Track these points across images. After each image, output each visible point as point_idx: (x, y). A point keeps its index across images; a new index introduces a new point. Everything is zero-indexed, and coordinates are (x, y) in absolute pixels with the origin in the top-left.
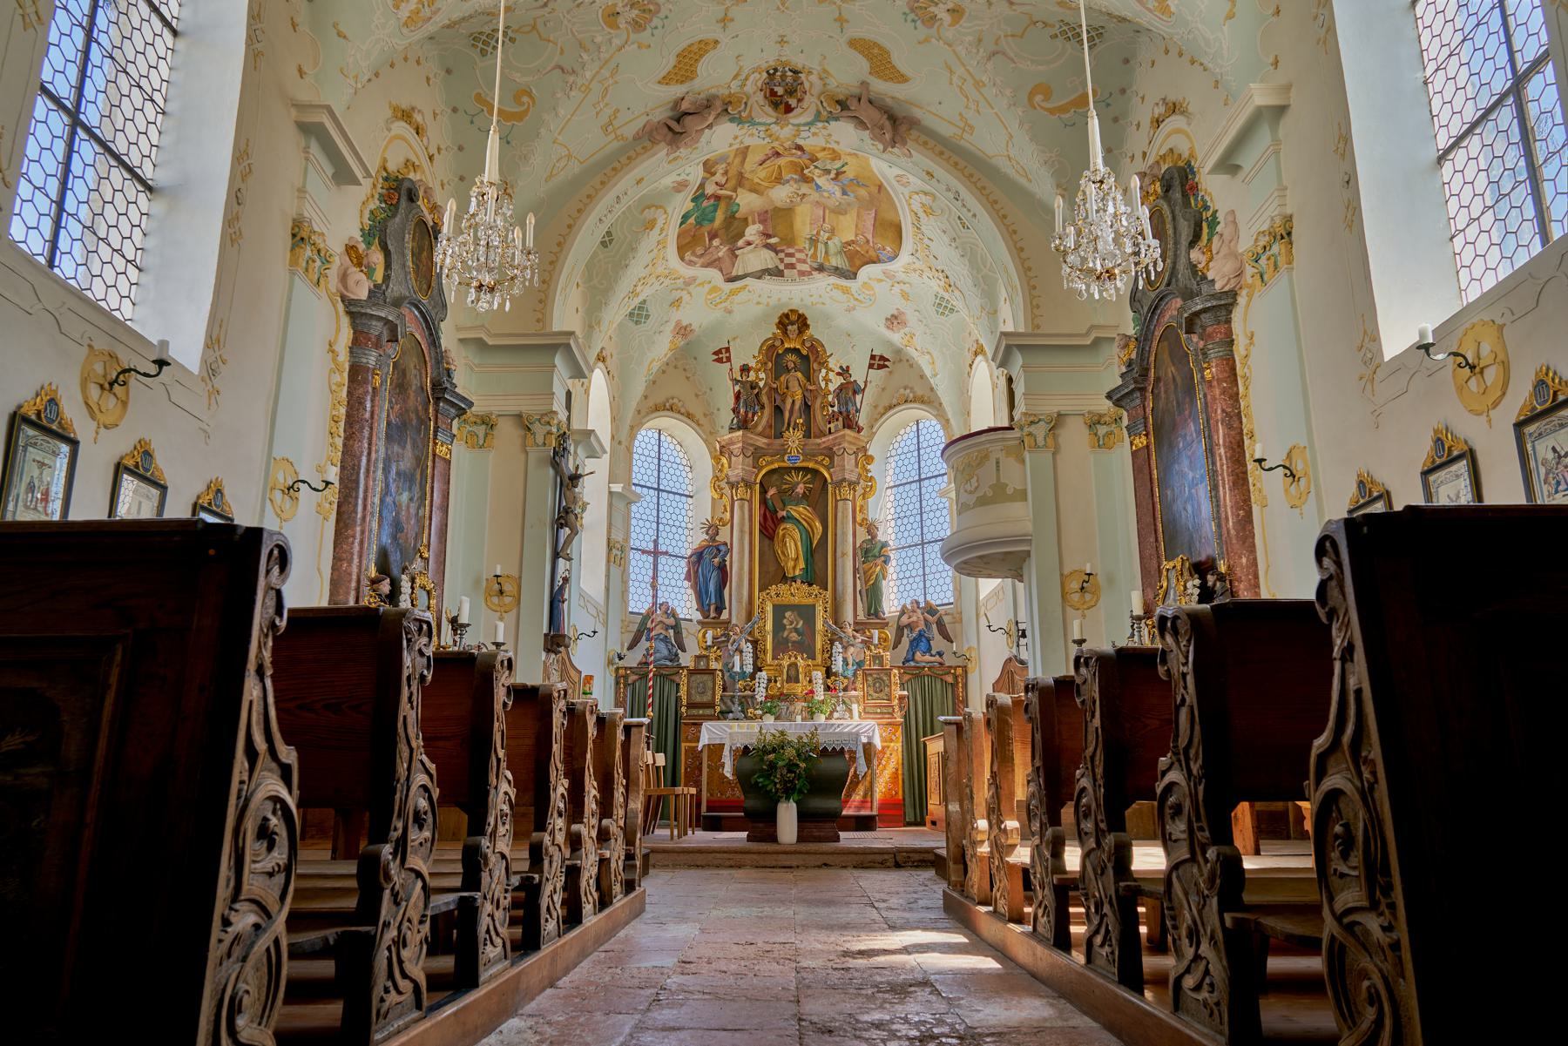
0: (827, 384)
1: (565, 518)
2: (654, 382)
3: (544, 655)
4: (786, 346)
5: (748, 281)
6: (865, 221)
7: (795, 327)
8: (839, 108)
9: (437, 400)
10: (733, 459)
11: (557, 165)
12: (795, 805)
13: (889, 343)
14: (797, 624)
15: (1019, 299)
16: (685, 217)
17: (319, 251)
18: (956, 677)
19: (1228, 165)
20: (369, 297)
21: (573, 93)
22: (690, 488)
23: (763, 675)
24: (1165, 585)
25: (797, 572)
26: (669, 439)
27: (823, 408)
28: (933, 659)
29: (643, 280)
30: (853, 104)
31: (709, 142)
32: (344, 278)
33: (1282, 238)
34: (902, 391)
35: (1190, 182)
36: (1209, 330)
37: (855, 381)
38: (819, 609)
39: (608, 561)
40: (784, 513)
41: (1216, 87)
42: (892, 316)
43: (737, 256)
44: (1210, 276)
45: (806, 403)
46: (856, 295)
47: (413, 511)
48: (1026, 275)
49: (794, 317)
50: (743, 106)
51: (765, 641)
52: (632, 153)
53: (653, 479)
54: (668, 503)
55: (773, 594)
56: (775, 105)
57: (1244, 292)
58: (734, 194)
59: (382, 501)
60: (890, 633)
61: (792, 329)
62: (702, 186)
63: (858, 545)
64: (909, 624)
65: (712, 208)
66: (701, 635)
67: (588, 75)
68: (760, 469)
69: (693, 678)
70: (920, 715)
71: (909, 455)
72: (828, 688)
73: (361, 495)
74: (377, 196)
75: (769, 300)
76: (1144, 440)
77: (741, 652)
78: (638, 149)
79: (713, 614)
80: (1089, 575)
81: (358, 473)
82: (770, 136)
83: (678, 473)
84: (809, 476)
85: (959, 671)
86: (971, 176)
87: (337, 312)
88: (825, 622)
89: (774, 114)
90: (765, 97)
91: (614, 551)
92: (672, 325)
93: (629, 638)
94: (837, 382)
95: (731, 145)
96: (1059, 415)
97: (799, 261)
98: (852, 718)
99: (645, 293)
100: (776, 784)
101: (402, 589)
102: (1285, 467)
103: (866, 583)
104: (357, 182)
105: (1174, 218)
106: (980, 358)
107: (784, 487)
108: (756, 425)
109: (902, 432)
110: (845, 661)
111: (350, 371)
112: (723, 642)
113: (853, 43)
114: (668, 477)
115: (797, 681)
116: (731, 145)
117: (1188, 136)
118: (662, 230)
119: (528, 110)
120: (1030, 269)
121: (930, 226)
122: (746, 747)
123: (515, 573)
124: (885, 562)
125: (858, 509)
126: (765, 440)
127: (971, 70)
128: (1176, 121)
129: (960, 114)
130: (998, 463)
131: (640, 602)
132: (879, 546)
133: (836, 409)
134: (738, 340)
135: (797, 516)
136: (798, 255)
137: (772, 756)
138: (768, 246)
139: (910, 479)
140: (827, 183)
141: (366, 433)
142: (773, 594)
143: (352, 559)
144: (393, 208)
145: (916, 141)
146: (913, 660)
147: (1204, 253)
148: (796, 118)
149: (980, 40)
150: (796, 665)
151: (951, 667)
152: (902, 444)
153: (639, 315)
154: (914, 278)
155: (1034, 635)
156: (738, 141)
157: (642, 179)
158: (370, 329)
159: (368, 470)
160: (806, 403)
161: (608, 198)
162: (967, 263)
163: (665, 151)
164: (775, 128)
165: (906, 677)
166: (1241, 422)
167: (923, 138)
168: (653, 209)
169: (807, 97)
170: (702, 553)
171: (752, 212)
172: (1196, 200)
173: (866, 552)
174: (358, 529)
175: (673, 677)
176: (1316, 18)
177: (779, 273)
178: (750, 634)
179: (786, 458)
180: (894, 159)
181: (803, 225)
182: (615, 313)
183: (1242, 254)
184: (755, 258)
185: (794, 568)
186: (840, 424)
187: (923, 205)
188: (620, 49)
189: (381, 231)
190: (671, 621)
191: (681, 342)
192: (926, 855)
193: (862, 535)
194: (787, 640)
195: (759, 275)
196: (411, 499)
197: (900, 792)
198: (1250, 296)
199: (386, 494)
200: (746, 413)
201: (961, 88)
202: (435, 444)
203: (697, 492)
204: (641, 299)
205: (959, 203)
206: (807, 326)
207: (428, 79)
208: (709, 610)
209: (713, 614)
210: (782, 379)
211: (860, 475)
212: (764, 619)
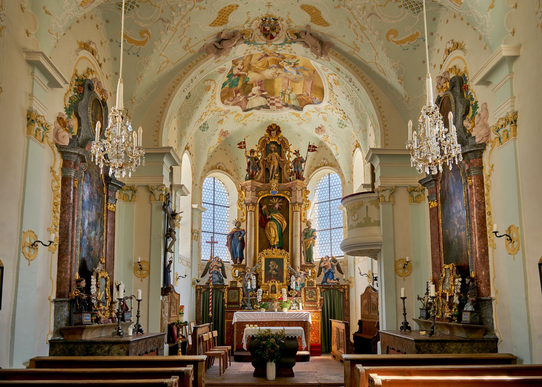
0: (289, 158)
1: (170, 234)
2: (211, 156)
3: (161, 297)
4: (271, 140)
5: (254, 111)
6: (307, 86)
7: (275, 132)
8: (296, 37)
9: (107, 184)
10: (247, 192)
11: (162, 66)
12: (274, 364)
13: (317, 139)
14: (275, 267)
15: (379, 131)
16: (224, 85)
17: (42, 125)
18: (344, 290)
19: (485, 81)
20: (70, 143)
21: (168, 32)
24: (444, 275)
25: (275, 243)
28: (334, 282)
29: (205, 114)
30: (303, 36)
31: (234, 53)
32: (56, 135)
33: (512, 123)
34: (322, 160)
35: (464, 85)
36: (471, 161)
37: (302, 157)
38: (285, 260)
39: (192, 239)
40: (270, 217)
41: (480, 39)
42: (319, 127)
43: (248, 100)
44: (473, 134)
46: (302, 118)
47: (97, 239)
48: (382, 120)
49: (274, 127)
50: (250, 36)
52: (198, 58)
53: (211, 200)
54: (218, 210)
55: (265, 253)
56: (266, 35)
57: (490, 144)
58: (247, 73)
59: (81, 239)
60: (316, 270)
61: (274, 133)
62: (232, 70)
63: (302, 231)
65: (236, 80)
66: (233, 271)
67: (176, 23)
68: (259, 197)
69: (230, 291)
70: (329, 306)
71: (325, 189)
72: (289, 296)
73: (70, 240)
74: (73, 90)
76: (435, 203)
77: (251, 279)
78: (201, 56)
79: (238, 262)
80: (408, 262)
81: (68, 230)
82: (263, 49)
83: (222, 196)
84: (281, 200)
85: (346, 287)
86: (358, 71)
87: (54, 152)
89: (265, 40)
90: (261, 31)
91: (194, 234)
92: (219, 131)
93: (201, 272)
95: (245, 54)
96: (396, 187)
97: (277, 102)
98: (299, 309)
99: (206, 118)
100: (266, 355)
101: (92, 283)
102: (507, 235)
104: (61, 87)
105: (455, 102)
106: (358, 149)
107: (270, 205)
108: (257, 177)
110: (296, 283)
111: (62, 180)
112: (243, 274)
113: (303, 7)
114: (218, 199)
116: (245, 54)
117: (464, 61)
118: (213, 91)
119: (147, 40)
120: (384, 117)
121: (337, 90)
122: (253, 336)
123: (147, 260)
124: (314, 239)
125: (302, 214)
126: (261, 184)
127: (360, 22)
128: (457, 53)
129: (354, 42)
130: (367, 208)
131: (206, 256)
133: (293, 170)
134: (249, 137)
135: (275, 218)
136: (276, 100)
137: (264, 342)
138: (262, 96)
139: (326, 200)
140: (290, 69)
141: (71, 210)
142: (265, 253)
143: (67, 271)
144: (81, 95)
145: (332, 53)
147: (470, 122)
148: (275, 42)
149: (364, 8)
150: (275, 285)
151: (342, 285)
152: (322, 184)
153: (204, 127)
154: (329, 112)
155: (381, 281)
156: (248, 52)
157: (203, 71)
158: (71, 159)
159: (73, 228)
161: (188, 80)
162: (354, 107)
163: (214, 58)
164: (265, 46)
165: (323, 290)
166: (485, 207)
167: (336, 52)
168: (209, 81)
169: (281, 32)
171: (255, 81)
172: (467, 94)
173: (306, 234)
174: (70, 257)
176: (537, 13)
177: (267, 107)
178: (255, 271)
179: (271, 192)
180: (322, 61)
181: (279, 86)
182: (192, 129)
183: (490, 127)
184: (257, 101)
185: (274, 241)
187: (334, 80)
188: (190, 10)
189: (75, 108)
190: (220, 265)
191: (223, 138)
193: (304, 226)
194: (271, 274)
195: (258, 108)
196: (96, 234)
197: (320, 341)
198: (493, 147)
199: (83, 235)
200: (253, 172)
201: (354, 30)
202: (107, 205)
204: (204, 122)
205: (352, 84)
206: (280, 132)
207: (97, 26)
208: (237, 260)
209: (238, 262)
210: (269, 156)
211: (303, 200)
212: (261, 265)
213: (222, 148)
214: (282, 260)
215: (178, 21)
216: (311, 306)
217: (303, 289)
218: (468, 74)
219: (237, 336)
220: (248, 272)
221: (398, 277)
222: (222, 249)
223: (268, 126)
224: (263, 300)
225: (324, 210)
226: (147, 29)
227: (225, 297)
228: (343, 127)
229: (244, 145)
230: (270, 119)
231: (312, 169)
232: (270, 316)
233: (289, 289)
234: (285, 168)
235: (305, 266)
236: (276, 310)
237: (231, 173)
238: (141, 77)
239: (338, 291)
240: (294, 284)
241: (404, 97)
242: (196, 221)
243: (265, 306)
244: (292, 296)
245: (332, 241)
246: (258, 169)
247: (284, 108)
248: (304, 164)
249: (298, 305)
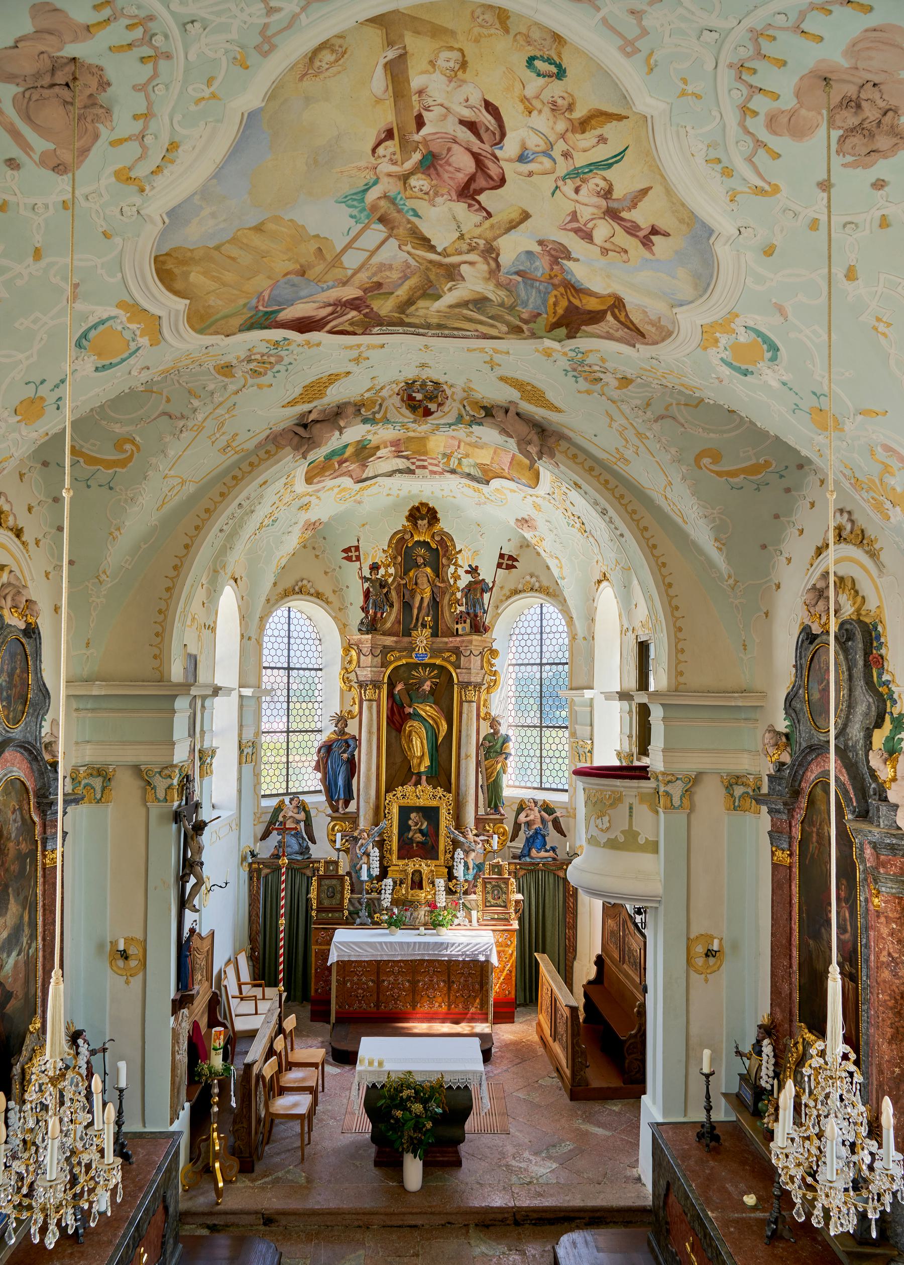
7: (425, 522)
14: (422, 825)
23: (389, 882)
26: (299, 615)
28: (547, 854)
34: (528, 578)
38: (443, 813)
39: (240, 763)
40: (411, 710)
42: (523, 519)
49: (424, 511)
50: (377, 408)
55: (399, 794)
70: (533, 907)
72: (450, 892)
77: (368, 855)
84: (436, 672)
86: (622, 496)
90: (403, 400)
93: (261, 829)
94: (465, 580)
97: (431, 464)
100: (402, 1144)
115: (421, 888)
123: (139, 936)
124: (506, 759)
125: (482, 703)
126: (394, 639)
130: (631, 808)
131: (272, 782)
132: (501, 741)
134: (367, 527)
135: (423, 714)
139: (532, 661)
142: (399, 794)
145: (566, 452)
146: (529, 855)
149: (648, 405)
167: (574, 450)
169: (448, 402)
170: (331, 745)
175: (304, 871)
186: (467, 626)
192: (544, 1214)
195: (391, 474)
197: (513, 992)
200: (375, 613)
202: (44, 856)
203: (325, 667)
206: (438, 520)
210: (411, 574)
213: (308, 545)
214: (436, 810)
215: (206, 414)
218: (884, 628)
219: (337, 991)
221: (694, 976)
223: (410, 508)
226: (131, 435)
227: (313, 895)
229: (357, 553)
230: (415, 491)
231: (504, 592)
232: (408, 948)
233: (451, 877)
234: (446, 601)
237: (327, 599)
238: (119, 529)
239: (555, 874)
240: (461, 868)
241: (726, 577)
242: (249, 719)
244: (456, 892)
247: (448, 475)
248: (488, 594)
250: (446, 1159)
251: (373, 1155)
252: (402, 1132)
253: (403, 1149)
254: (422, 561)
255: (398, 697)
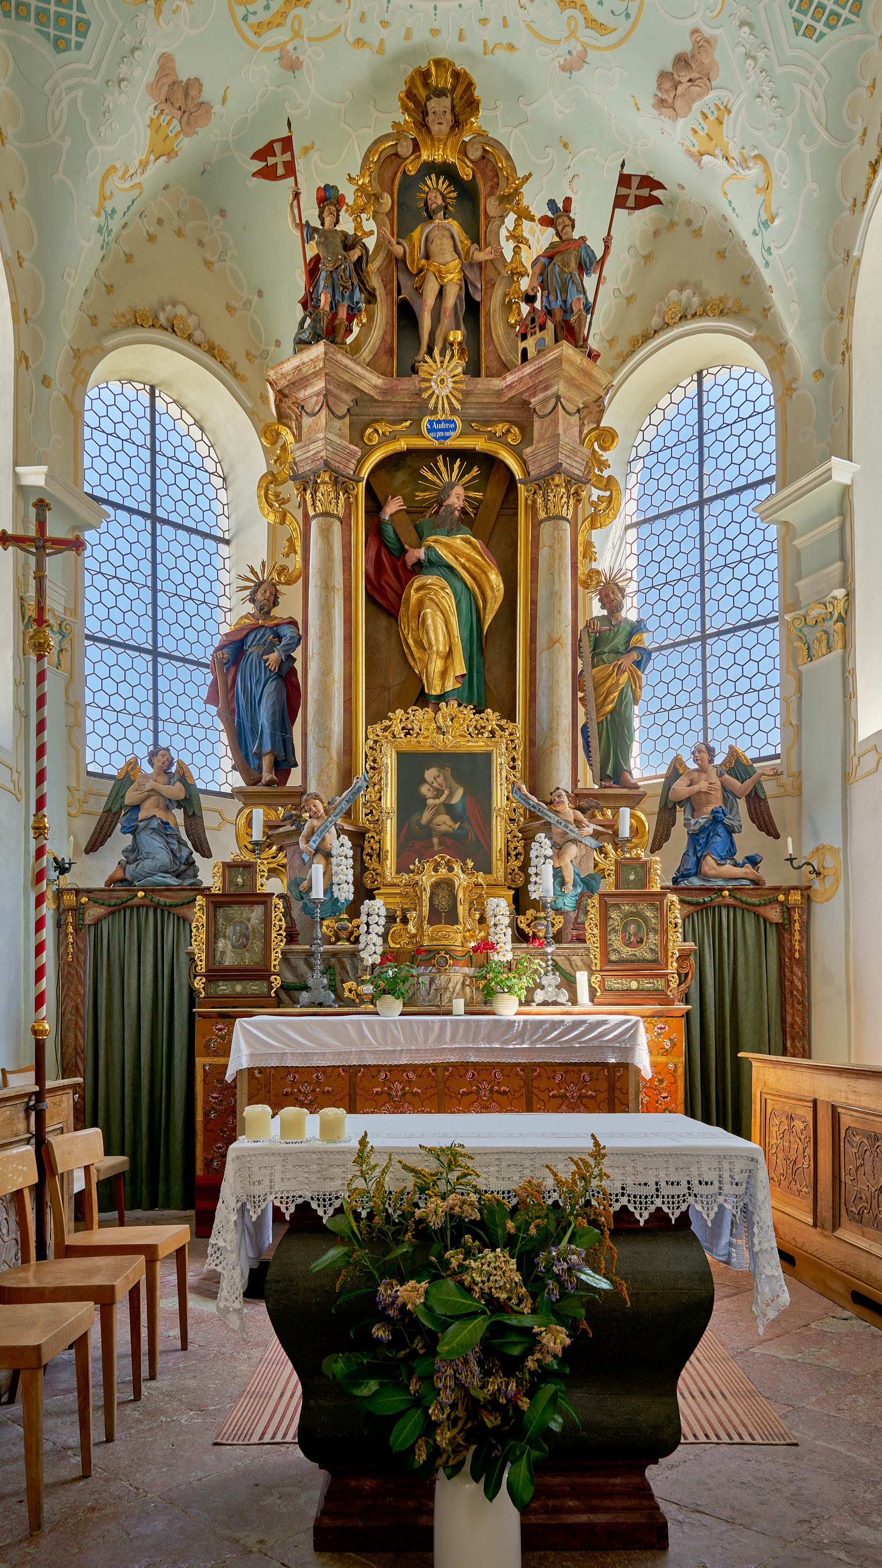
7: (446, 102)
14: (451, 795)
18: (788, 910)
22: (224, 523)
23: (377, 906)
25: (450, 685)
26: (174, 410)
27: (508, 307)
28: (738, 871)
34: (674, 293)
38: (500, 761)
40: (421, 553)
45: (469, 298)
51: (381, 832)
54: (176, 549)
55: (397, 728)
63: (581, 626)
64: (688, 799)
66: (242, 821)
68: (368, 450)
72: (520, 936)
75: (384, 33)
77: (328, 856)
84: (475, 471)
85: (795, 897)
88: (514, 788)
93: (86, 827)
98: (574, 1000)
100: (430, 1427)
103: (599, 707)
107: (420, 495)
109: (663, 403)
112: (288, 834)
115: (453, 919)
122: (304, 1208)
124: (638, 664)
125: (580, 549)
135: (450, 560)
142: (397, 728)
146: (698, 873)
151: (777, 889)
160: (469, 298)
170: (242, 642)
178: (348, 814)
185: (444, 674)
190: (177, 791)
194: (428, 830)
200: (334, 305)
203: (237, 533)
206: (472, 105)
208: (260, 768)
209: (267, 776)
210: (416, 234)
212: (376, 784)
216: (634, 985)
217: (596, 899)
220: (315, 816)
222: (199, 733)
224: (387, 957)
225: (673, 550)
227: (198, 947)
228: (820, 27)
229: (287, 157)
235: (596, 796)
236: (459, 1005)
239: (757, 916)
243: (402, 988)
244: (535, 937)
245: (712, 692)
246: (358, 296)
248: (595, 277)
249: (569, 983)
250: (602, 1518)
251: (313, 1512)
252: (428, 1379)
253: (435, 1452)
254: (440, 201)
255: (389, 530)
